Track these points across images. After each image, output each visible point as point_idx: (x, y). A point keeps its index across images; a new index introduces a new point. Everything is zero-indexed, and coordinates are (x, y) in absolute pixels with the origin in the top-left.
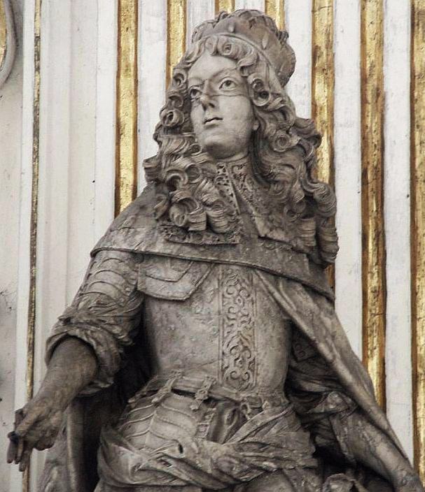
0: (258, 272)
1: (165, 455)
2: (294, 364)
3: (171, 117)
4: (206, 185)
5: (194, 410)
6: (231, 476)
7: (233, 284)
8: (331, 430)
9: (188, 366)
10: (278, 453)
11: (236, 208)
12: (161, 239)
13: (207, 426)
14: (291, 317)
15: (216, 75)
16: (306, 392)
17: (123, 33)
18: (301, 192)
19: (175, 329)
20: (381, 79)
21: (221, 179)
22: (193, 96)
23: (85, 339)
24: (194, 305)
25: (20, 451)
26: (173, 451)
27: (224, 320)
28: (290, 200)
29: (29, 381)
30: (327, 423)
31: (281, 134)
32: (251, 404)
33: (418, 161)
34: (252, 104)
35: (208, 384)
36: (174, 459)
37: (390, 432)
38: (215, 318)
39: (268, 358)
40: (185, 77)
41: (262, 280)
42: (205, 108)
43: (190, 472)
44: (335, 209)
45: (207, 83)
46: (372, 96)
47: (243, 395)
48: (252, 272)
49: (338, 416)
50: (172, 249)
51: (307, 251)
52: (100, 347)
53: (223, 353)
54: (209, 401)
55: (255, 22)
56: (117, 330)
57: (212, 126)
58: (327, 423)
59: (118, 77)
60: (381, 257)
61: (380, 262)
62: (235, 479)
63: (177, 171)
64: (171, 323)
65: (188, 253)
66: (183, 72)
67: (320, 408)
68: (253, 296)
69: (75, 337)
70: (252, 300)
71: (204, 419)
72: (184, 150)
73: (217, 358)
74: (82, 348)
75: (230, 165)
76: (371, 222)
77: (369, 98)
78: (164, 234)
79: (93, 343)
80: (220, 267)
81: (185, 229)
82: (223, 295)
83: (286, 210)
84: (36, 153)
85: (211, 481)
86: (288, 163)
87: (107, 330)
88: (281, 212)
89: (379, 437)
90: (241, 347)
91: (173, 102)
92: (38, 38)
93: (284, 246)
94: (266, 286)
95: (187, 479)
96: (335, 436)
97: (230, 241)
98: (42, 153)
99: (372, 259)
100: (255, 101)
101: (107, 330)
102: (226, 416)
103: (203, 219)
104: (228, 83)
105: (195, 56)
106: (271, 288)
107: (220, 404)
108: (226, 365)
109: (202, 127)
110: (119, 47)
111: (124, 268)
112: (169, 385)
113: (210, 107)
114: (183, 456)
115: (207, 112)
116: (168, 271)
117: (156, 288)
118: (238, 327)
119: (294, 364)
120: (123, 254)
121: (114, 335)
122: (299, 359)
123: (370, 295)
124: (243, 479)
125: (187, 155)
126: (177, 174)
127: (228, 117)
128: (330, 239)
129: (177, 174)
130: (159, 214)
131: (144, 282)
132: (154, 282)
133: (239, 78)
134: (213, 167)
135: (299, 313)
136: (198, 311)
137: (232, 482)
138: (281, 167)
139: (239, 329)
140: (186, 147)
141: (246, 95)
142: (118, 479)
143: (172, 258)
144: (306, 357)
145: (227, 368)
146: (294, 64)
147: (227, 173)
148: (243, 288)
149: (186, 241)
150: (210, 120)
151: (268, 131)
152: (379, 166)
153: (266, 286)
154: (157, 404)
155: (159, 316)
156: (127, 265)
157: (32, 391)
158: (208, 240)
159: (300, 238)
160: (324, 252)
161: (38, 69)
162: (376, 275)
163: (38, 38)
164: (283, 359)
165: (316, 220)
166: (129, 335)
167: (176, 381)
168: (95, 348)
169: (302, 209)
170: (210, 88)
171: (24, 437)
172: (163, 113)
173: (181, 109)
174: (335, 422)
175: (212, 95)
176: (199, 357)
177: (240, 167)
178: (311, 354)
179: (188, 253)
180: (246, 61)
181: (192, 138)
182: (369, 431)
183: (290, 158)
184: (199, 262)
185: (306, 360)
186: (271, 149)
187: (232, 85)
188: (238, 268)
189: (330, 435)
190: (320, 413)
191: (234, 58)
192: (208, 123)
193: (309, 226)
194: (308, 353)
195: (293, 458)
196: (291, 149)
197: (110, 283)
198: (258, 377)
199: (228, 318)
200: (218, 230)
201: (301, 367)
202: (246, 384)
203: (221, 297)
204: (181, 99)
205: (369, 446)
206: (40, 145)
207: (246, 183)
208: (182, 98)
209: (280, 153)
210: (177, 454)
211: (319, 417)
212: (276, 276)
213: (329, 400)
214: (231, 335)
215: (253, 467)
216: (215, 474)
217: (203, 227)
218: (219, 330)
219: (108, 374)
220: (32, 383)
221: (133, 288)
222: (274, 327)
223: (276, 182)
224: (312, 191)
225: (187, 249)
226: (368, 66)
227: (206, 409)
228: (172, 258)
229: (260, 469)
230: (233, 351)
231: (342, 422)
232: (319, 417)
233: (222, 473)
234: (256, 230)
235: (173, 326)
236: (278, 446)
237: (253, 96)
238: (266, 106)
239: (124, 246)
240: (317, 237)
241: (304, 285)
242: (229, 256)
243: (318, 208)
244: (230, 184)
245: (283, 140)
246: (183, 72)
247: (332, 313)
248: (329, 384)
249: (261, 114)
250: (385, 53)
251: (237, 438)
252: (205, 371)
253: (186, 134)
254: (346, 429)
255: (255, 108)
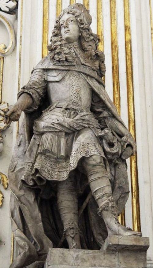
0: (82, 74)
1: (53, 123)
2: (93, 103)
3: (55, 32)
4: (65, 49)
5: (62, 111)
6: (74, 128)
7: (74, 76)
8: (105, 122)
9: (60, 100)
10: (88, 122)
11: (74, 55)
12: (52, 64)
13: (66, 115)
14: (92, 87)
15: (68, 19)
16: (97, 112)
17: (44, 33)
18: (94, 52)
19: (56, 90)
20: (117, 43)
21: (70, 48)
22: (61, 26)
23: (29, 92)
24: (62, 82)
25: (8, 121)
26: (56, 121)
27: (71, 86)
28: (91, 55)
29: (17, 126)
30: (104, 121)
31: (88, 36)
32: (80, 110)
33: (128, 64)
34: (79, 27)
35: (67, 104)
36: (56, 123)
37: (123, 123)
38: (68, 85)
39: (85, 99)
40: (59, 21)
41: (83, 76)
42: (65, 28)
43: (61, 127)
44: (104, 59)
45: (65, 21)
46: (114, 47)
47: (77, 108)
48: (80, 74)
49: (107, 118)
50: (55, 67)
51: (97, 70)
52: (33, 95)
53: (71, 95)
54: (66, 109)
55: (79, 6)
56: (38, 90)
57: (67, 33)
58: (104, 121)
59: (43, 44)
60: (118, 89)
61: (118, 90)
62: (75, 129)
63: (56, 45)
64: (55, 88)
65: (60, 68)
66: (59, 20)
67: (101, 116)
68: (80, 80)
69: (26, 93)
70: (80, 81)
71: (65, 113)
72: (59, 40)
73: (69, 97)
74: (28, 95)
75: (73, 45)
76: (115, 80)
77: (114, 48)
78: (53, 63)
79: (31, 93)
80: (70, 72)
81: (59, 61)
82: (71, 79)
83: (90, 58)
84: (20, 66)
85: (68, 130)
86: (91, 45)
87: (36, 90)
88: (88, 59)
89: (119, 124)
90: (77, 93)
91: (56, 29)
92: (21, 37)
93: (89, 67)
94: (84, 78)
95: (60, 129)
96: (106, 124)
97: (73, 64)
98: (22, 66)
99: (116, 90)
100: (80, 26)
101: (36, 90)
102: (72, 113)
103: (65, 57)
104: (72, 21)
105: (62, 15)
106: (86, 79)
107: (71, 110)
108: (72, 98)
109: (64, 34)
110: (43, 37)
111: (41, 74)
112: (54, 106)
113: (66, 27)
114: (59, 122)
115: (66, 29)
116: (54, 73)
117: (50, 79)
118: (75, 88)
119: (93, 103)
120: (40, 70)
121: (38, 92)
122: (95, 102)
123: (115, 99)
124: (78, 129)
125: (60, 41)
126: (56, 46)
127: (72, 31)
128: (104, 67)
129: (56, 46)
130: (51, 58)
131: (47, 77)
132: (50, 77)
133: (75, 20)
134: (68, 45)
135: (94, 86)
136: (63, 84)
137: (74, 130)
138: (88, 46)
139: (76, 88)
140: (59, 39)
141: (77, 24)
142: (39, 131)
143: (55, 70)
144: (97, 101)
145: (72, 99)
146: (91, 20)
147: (72, 47)
148: (77, 78)
149: (60, 64)
150: (66, 31)
151: (84, 35)
152: (117, 65)
153: (84, 78)
154: (51, 111)
155: (51, 87)
156: (42, 73)
157: (18, 129)
158: (66, 64)
159: (94, 66)
160: (102, 71)
161: (21, 44)
162: (117, 94)
163: (21, 37)
164: (90, 99)
165: (99, 61)
166: (43, 93)
167: (57, 104)
168: (32, 95)
169: (95, 58)
170: (66, 22)
171: (9, 117)
172: (53, 31)
173: (58, 30)
174: (106, 120)
175: (67, 24)
176: (64, 97)
177: (76, 45)
178: (98, 100)
179: (60, 68)
180: (76, 14)
181: (61, 37)
182: (116, 122)
183: (91, 43)
184: (63, 70)
185: (97, 102)
186: (85, 41)
187: (73, 21)
188: (75, 72)
189: (105, 124)
190: (101, 117)
191: (73, 14)
192: (66, 32)
193: (97, 63)
194: (98, 100)
195: (93, 125)
196: (91, 40)
197: (36, 77)
198: (82, 103)
199: (73, 85)
200: (69, 61)
201: (95, 104)
202: (78, 104)
203: (70, 80)
204: (58, 27)
205: (117, 127)
206: (21, 64)
207: (78, 50)
208: (58, 27)
209: (88, 42)
210: (57, 122)
211: (101, 119)
212: (87, 75)
213: (104, 113)
214: (73, 90)
215: (81, 126)
216: (69, 127)
217: (64, 59)
218: (70, 89)
219: (36, 104)
220: (18, 127)
221: (44, 79)
222: (87, 90)
223: (87, 51)
224: (97, 53)
225: (60, 67)
226: (113, 40)
227: (65, 111)
228: (55, 70)
229: (83, 126)
230: (74, 94)
231: (108, 120)
232: (101, 119)
233: (71, 127)
234: (81, 62)
235: (56, 89)
236: (88, 121)
237: (79, 25)
238: (83, 27)
239: (41, 67)
240: (99, 66)
241: (96, 79)
242: (72, 68)
243: (99, 57)
244: (73, 49)
245: (89, 38)
246: (59, 20)
247: (104, 89)
248: (104, 109)
249: (81, 30)
250: (118, 36)
251: (76, 118)
252: (65, 101)
253: (60, 37)
254: (109, 122)
255: (80, 28)
